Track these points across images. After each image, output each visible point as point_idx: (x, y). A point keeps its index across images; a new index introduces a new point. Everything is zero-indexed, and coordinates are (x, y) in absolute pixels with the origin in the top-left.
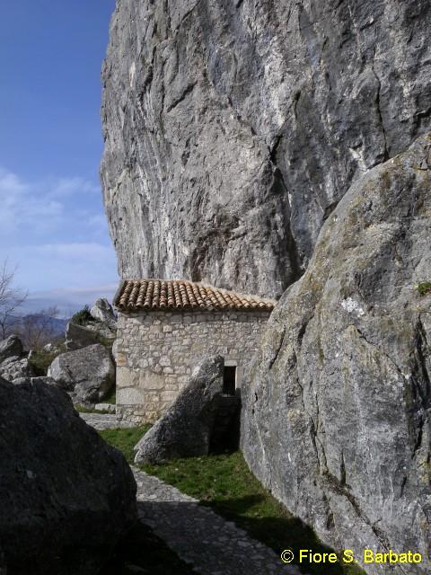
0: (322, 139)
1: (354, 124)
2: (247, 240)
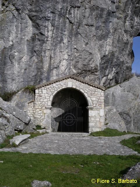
0: (112, 63)
1: (118, 64)
2: (97, 77)
